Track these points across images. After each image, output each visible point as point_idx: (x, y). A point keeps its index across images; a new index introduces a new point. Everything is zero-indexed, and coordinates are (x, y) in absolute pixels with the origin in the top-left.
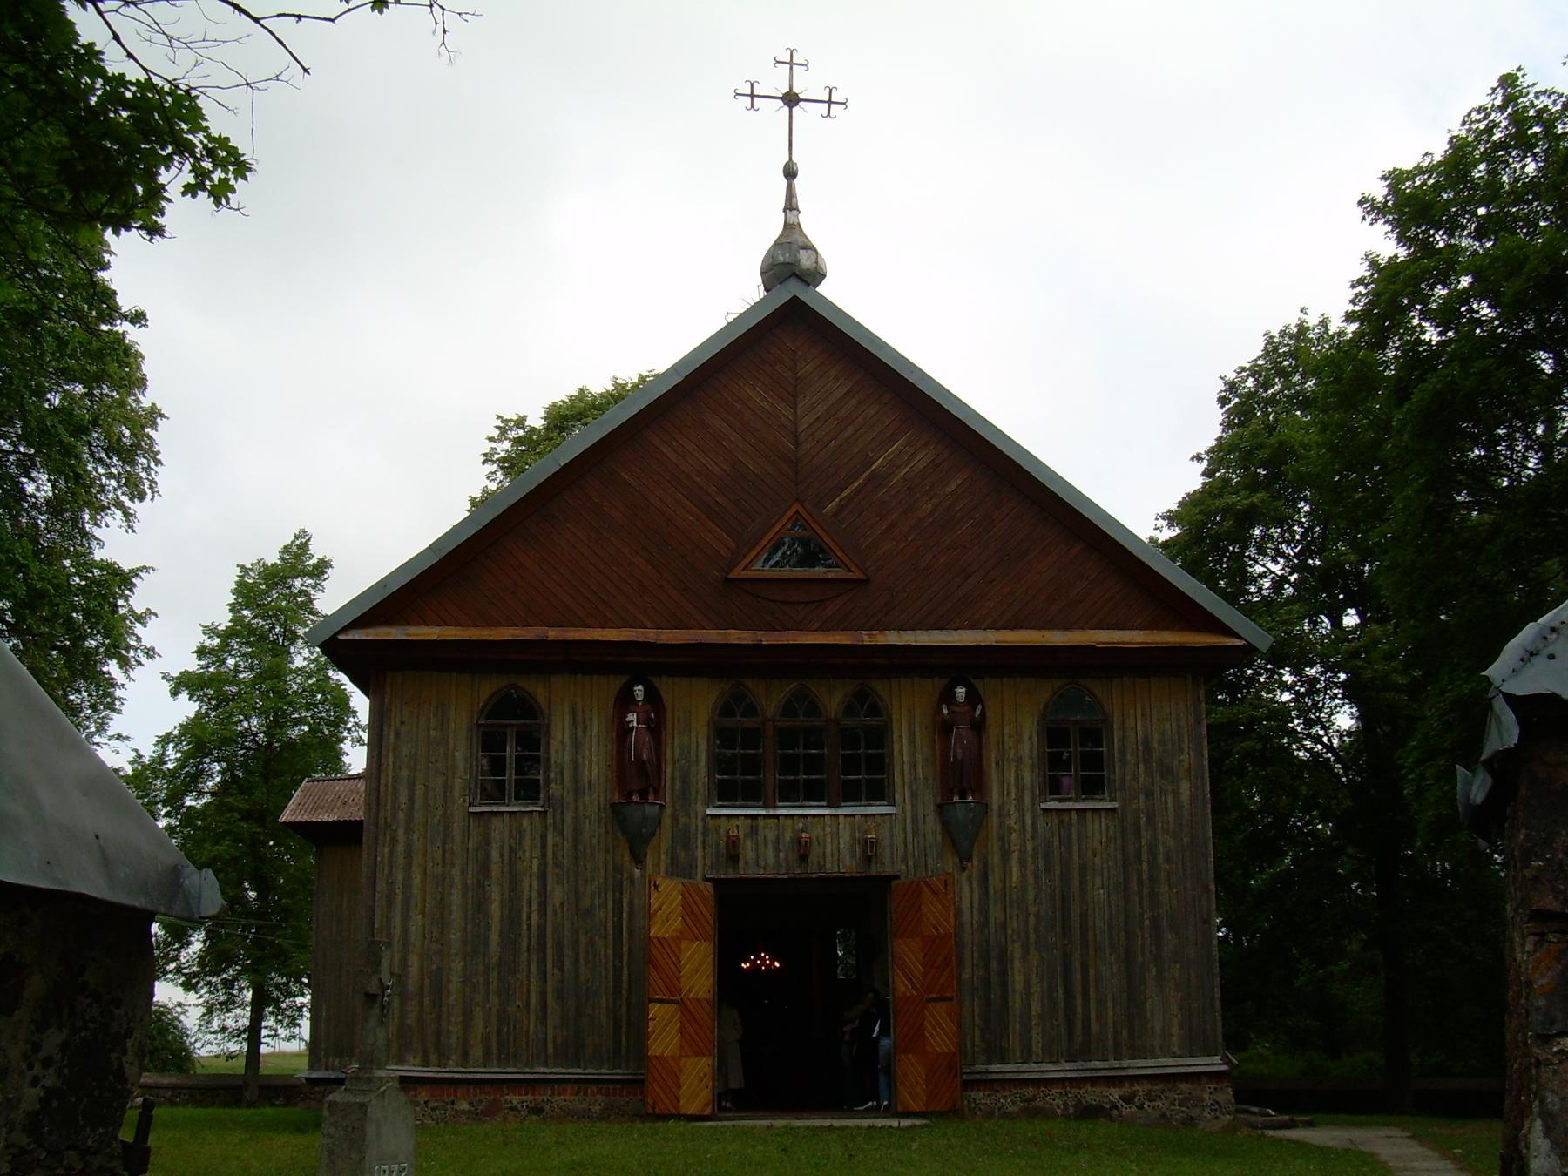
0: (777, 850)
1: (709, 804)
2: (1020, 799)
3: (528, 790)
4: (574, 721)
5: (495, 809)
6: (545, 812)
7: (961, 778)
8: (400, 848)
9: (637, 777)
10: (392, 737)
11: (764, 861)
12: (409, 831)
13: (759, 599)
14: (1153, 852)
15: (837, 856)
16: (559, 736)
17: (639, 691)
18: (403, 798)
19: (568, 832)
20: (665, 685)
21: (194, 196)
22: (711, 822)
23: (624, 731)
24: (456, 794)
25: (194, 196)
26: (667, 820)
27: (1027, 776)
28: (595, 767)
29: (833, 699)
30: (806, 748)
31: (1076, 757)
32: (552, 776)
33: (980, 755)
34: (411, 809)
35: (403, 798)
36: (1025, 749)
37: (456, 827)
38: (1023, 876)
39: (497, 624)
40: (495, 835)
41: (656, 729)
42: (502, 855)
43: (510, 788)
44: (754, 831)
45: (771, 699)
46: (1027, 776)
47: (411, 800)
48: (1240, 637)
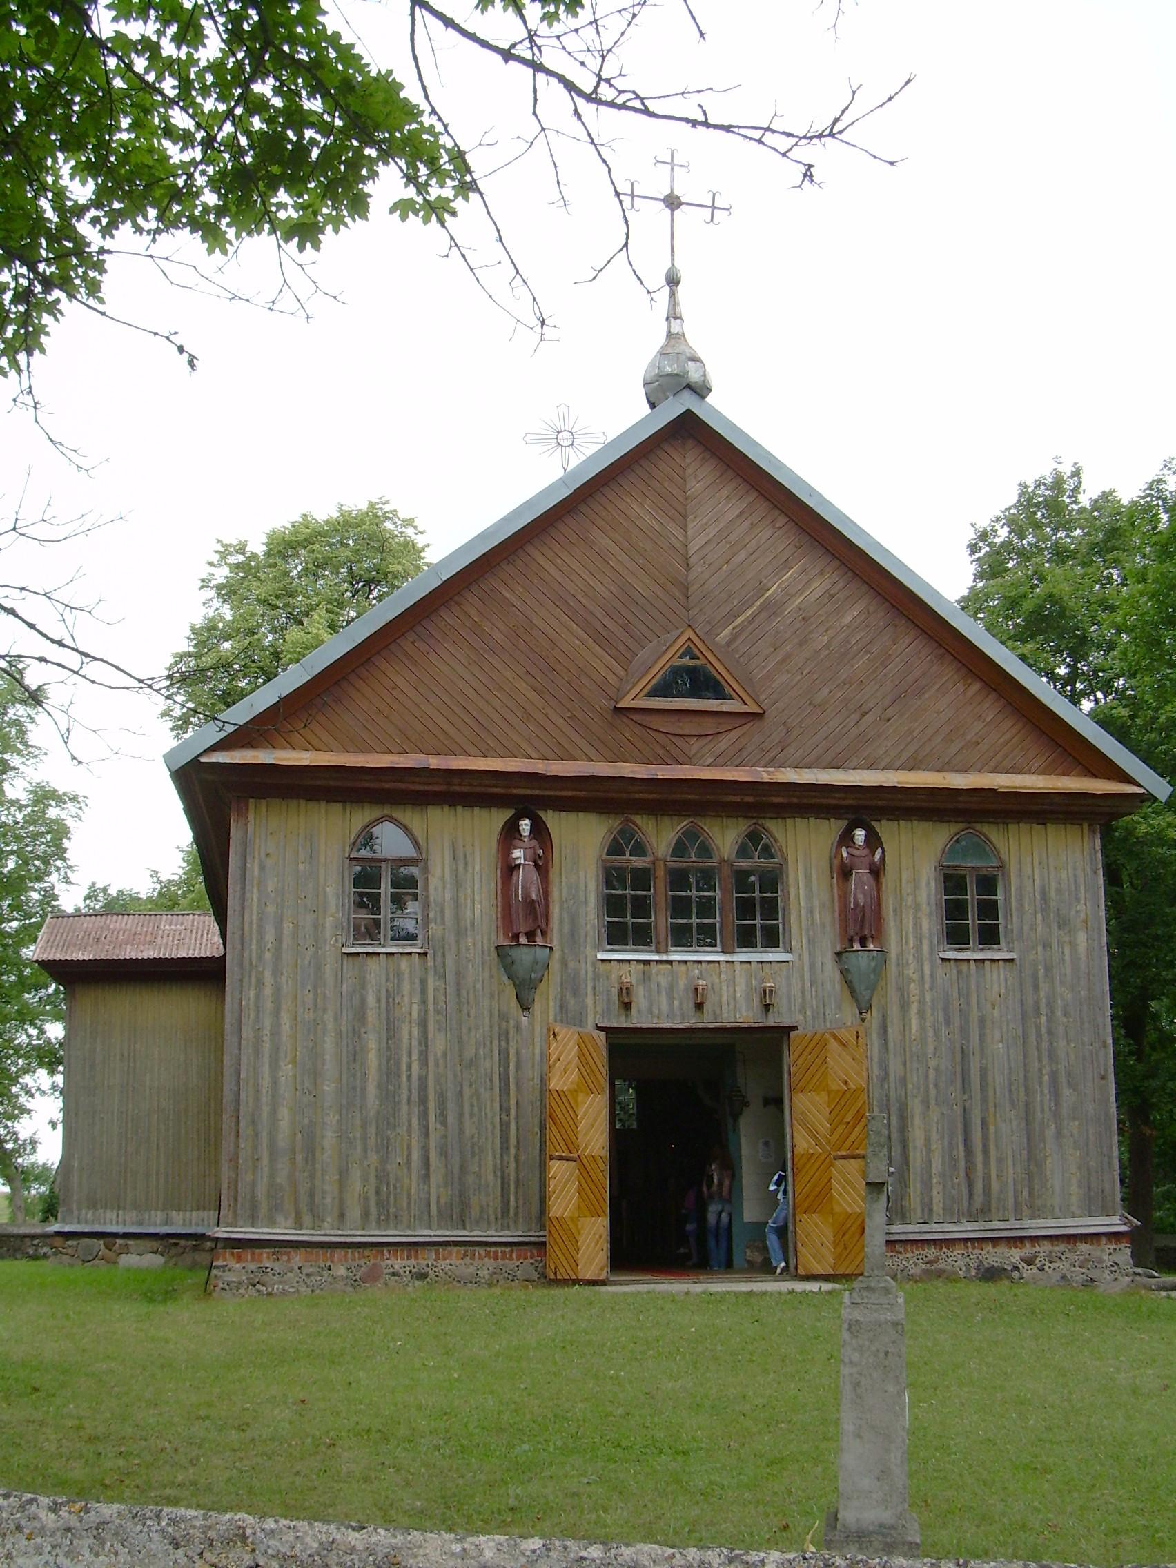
1: (598, 948)
2: (918, 947)
7: (861, 927)
8: (268, 991)
9: (525, 920)
11: (661, 1009)
12: (276, 973)
14: (1051, 1006)
15: (734, 1007)
18: (270, 937)
19: (450, 977)
20: (551, 819)
22: (602, 966)
23: (510, 869)
26: (555, 965)
29: (725, 839)
31: (971, 911)
32: (431, 915)
33: (879, 904)
35: (270, 937)
36: (923, 896)
38: (922, 1029)
40: (372, 979)
41: (542, 867)
44: (646, 978)
45: (661, 837)
47: (279, 939)
48: (1140, 786)
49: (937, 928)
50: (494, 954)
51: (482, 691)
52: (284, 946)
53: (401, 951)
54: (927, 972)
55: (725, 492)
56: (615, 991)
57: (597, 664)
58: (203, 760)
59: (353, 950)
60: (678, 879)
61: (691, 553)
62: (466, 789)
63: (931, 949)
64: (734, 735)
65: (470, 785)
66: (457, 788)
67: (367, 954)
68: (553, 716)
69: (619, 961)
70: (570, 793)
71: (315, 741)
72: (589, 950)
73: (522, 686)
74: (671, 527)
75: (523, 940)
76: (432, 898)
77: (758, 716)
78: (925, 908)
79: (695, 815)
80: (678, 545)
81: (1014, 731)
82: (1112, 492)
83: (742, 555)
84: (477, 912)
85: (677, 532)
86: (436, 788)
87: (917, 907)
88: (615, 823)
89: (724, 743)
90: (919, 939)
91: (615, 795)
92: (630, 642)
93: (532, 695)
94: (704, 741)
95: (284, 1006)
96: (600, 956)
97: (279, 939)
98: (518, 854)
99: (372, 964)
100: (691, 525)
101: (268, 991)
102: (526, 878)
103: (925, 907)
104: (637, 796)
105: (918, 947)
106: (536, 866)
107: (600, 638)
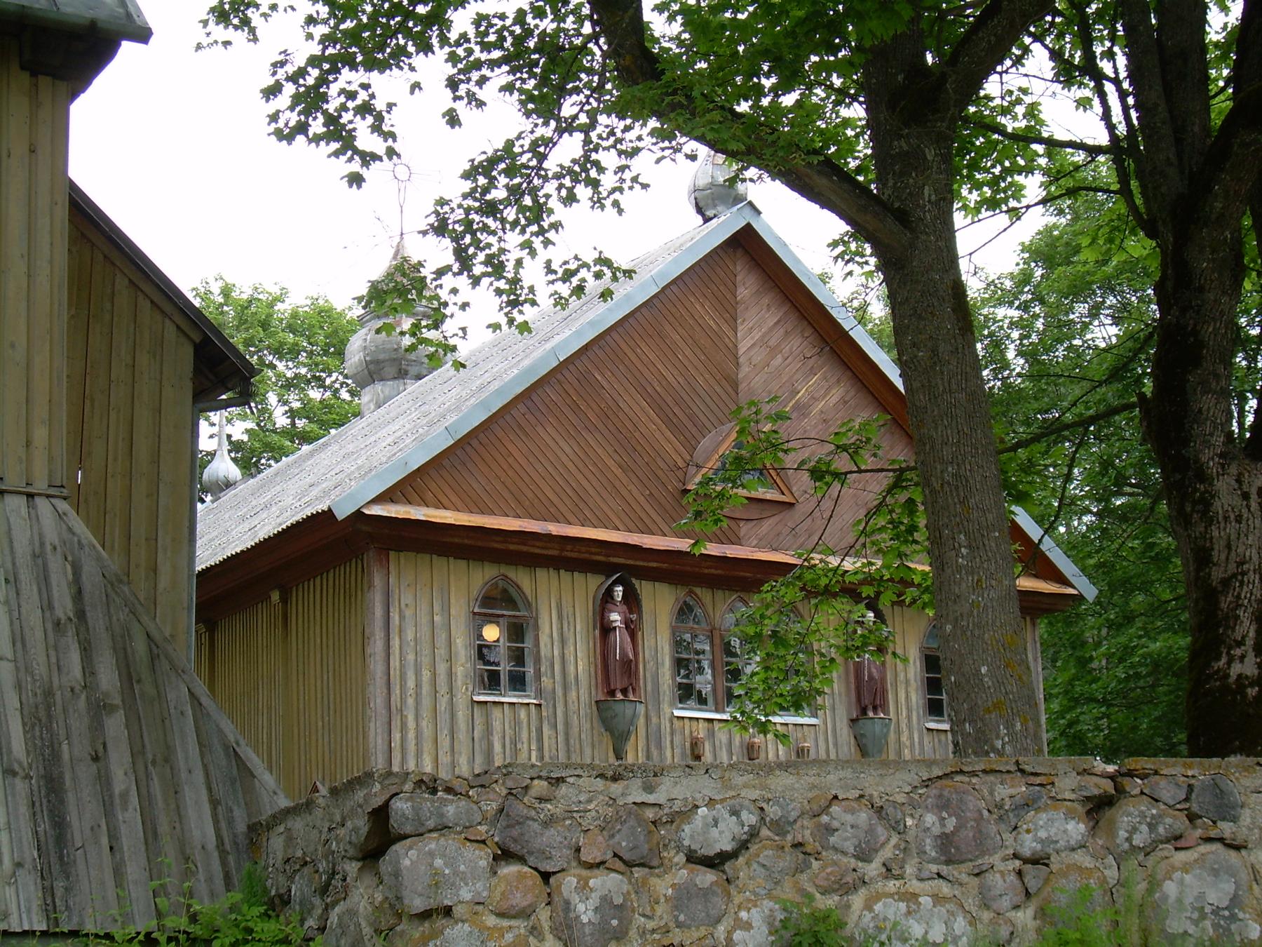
0: (730, 754)
1: (672, 705)
2: (909, 717)
3: (518, 682)
4: (560, 617)
5: (497, 699)
6: (540, 705)
8: (411, 735)
9: (617, 677)
10: (397, 618)
13: (702, 508)
16: (547, 630)
17: (619, 590)
18: (411, 684)
19: (560, 727)
20: (645, 589)
21: (318, 145)
22: (677, 723)
23: (606, 630)
24: (459, 683)
25: (318, 145)
26: (641, 721)
27: (914, 698)
28: (580, 663)
30: (1212, 253)
32: (543, 669)
34: (418, 695)
35: (411, 684)
36: (911, 675)
37: (462, 715)
39: (492, 513)
40: (497, 725)
41: (632, 629)
42: (504, 746)
43: (504, 679)
44: (711, 734)
46: (914, 698)
47: (418, 685)
48: (1073, 587)
49: (921, 702)
50: (594, 708)
51: (581, 466)
52: (424, 692)
53: (520, 701)
54: (916, 740)
55: (766, 301)
56: (688, 745)
57: (668, 448)
58: (367, 512)
59: (482, 698)
60: (1074, 648)
61: (740, 352)
62: (574, 555)
63: (919, 719)
64: (776, 519)
65: (579, 552)
66: (569, 554)
67: (494, 703)
68: (635, 492)
69: (690, 718)
70: (654, 565)
71: (445, 501)
72: (666, 708)
73: (611, 463)
74: (725, 327)
75: (619, 696)
76: (542, 654)
77: (791, 505)
78: (913, 685)
79: (742, 590)
80: (730, 345)
81: (433, 485)
82: (290, 144)
83: (779, 359)
84: (580, 668)
85: (731, 334)
86: (550, 552)
87: (907, 682)
88: (681, 593)
89: (766, 526)
90: (909, 709)
91: (688, 569)
92: (694, 430)
93: (618, 472)
94: (751, 524)
95: (425, 749)
96: (677, 713)
97: (418, 685)
98: (615, 617)
99: (496, 713)
100: (740, 328)
101: (411, 735)
102: (620, 638)
103: (912, 682)
104: (706, 571)
105: (909, 717)
106: (627, 627)
107: (669, 422)
